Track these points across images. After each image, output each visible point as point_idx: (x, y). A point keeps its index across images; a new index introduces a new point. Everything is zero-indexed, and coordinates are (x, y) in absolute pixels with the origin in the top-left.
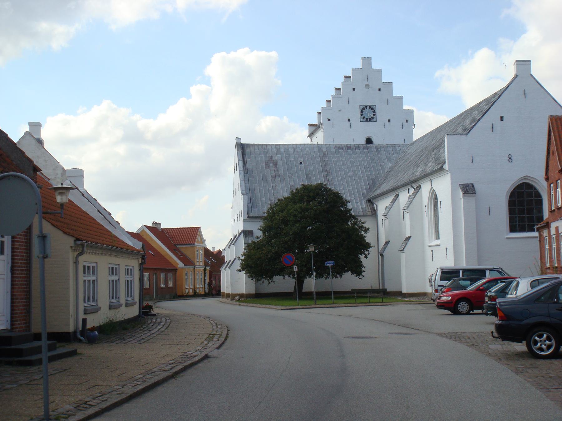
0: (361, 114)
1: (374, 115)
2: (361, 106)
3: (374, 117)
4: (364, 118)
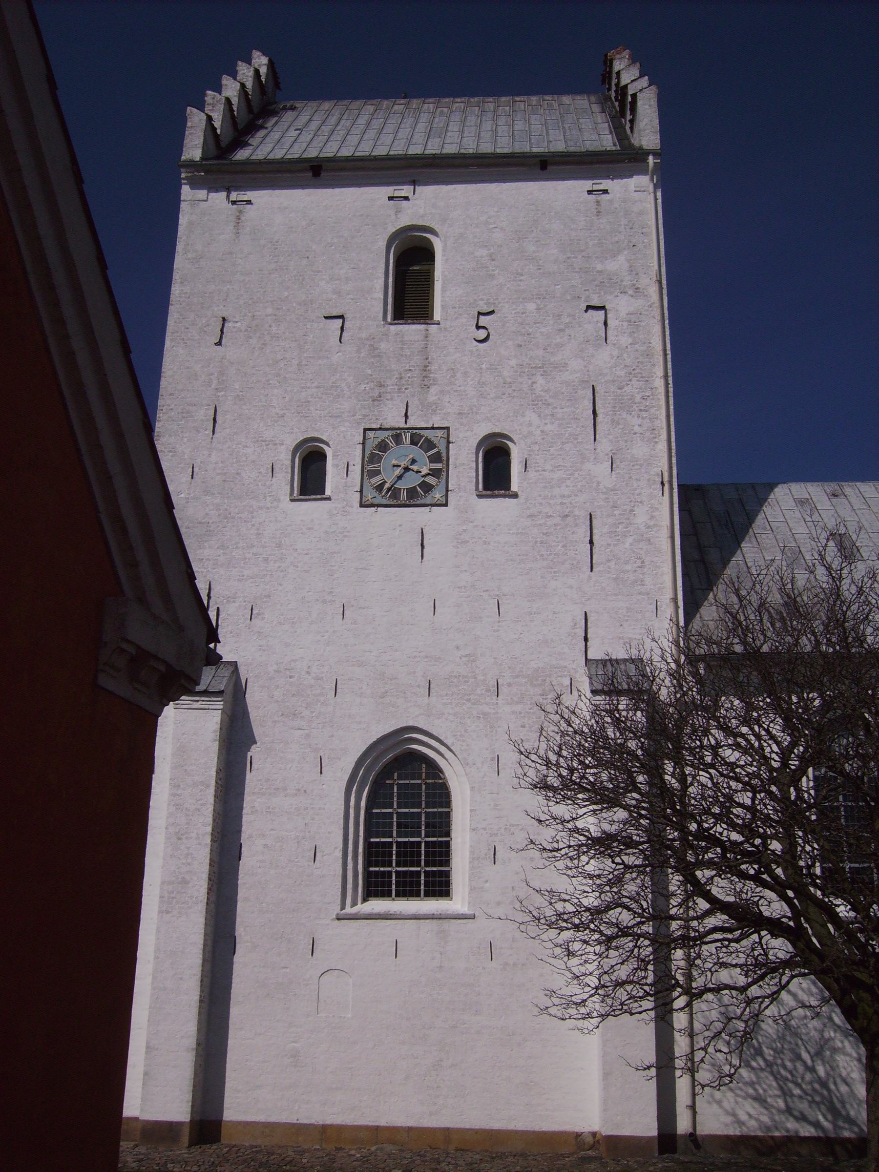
0: (371, 467)
1: (435, 473)
2: (371, 434)
3: (431, 480)
4: (380, 488)
